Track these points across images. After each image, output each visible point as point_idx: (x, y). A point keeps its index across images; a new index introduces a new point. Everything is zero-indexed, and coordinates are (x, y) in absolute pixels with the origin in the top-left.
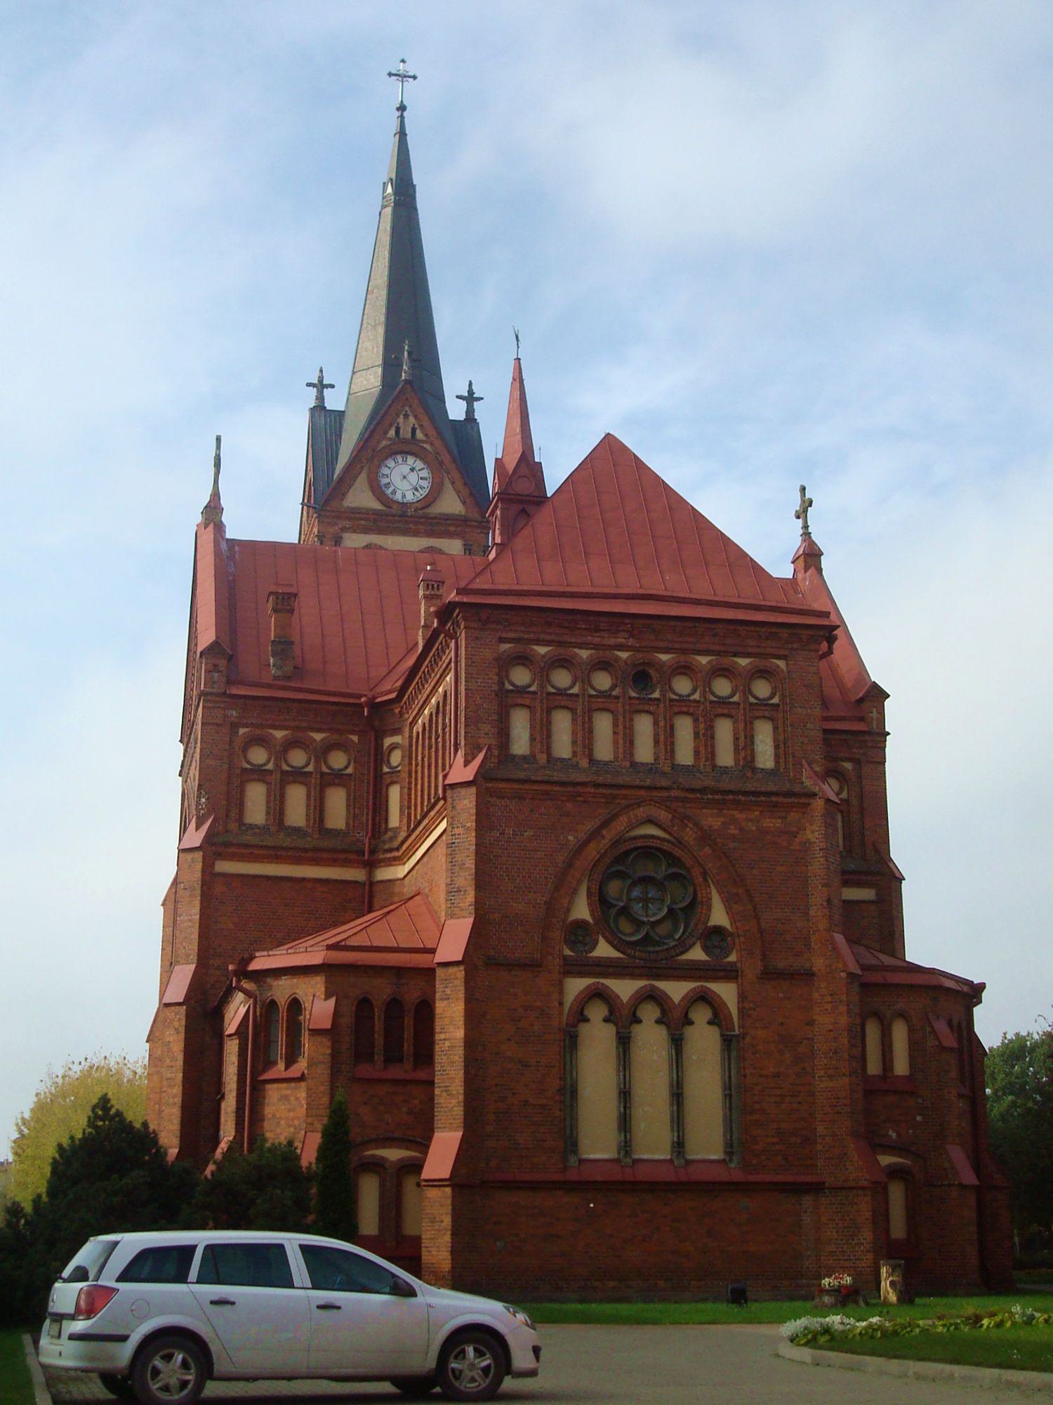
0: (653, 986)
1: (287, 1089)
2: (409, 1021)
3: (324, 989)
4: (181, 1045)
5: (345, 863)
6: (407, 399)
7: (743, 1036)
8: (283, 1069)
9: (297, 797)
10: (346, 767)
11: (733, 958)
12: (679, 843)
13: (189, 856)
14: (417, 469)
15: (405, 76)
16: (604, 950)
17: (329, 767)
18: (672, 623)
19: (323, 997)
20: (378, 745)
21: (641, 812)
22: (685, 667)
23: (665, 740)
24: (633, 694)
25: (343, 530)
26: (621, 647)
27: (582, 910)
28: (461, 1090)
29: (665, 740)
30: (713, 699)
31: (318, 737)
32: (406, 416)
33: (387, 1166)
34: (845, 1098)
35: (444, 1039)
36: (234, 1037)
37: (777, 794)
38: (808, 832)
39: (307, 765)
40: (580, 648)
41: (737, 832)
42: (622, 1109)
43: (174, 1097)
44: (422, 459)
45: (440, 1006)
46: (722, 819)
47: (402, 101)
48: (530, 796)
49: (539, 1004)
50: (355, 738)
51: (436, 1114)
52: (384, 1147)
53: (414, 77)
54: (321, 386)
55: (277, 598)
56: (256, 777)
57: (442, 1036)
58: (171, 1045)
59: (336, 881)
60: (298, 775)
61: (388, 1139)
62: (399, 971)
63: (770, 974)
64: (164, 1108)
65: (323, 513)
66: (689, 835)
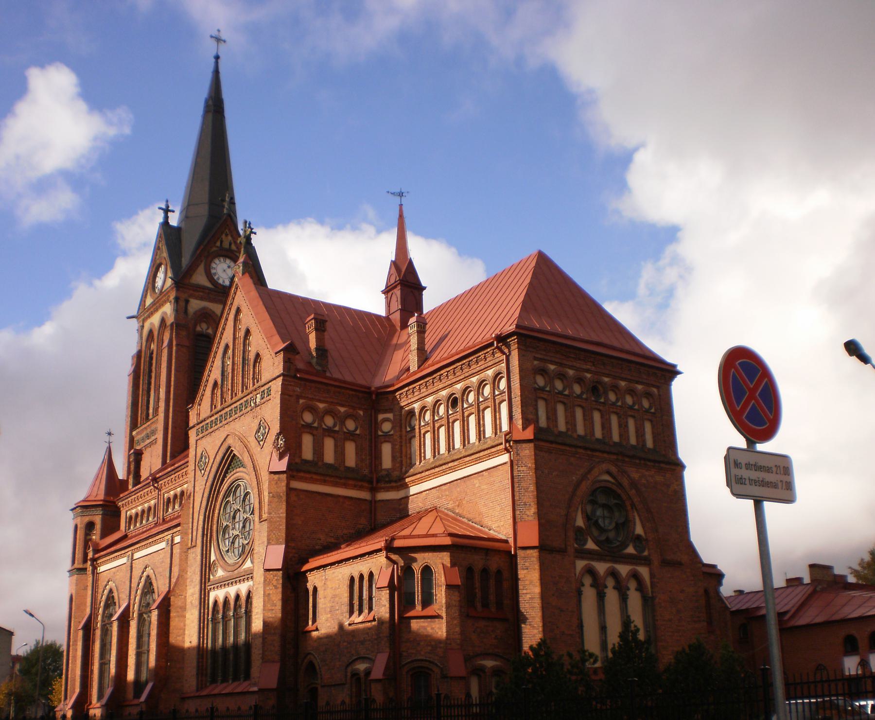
1: (424, 622)
2: (492, 582)
3: (449, 560)
4: (280, 596)
5: (360, 488)
6: (228, 225)
7: (653, 598)
8: (420, 610)
9: (329, 444)
10: (356, 430)
11: (646, 553)
12: (620, 485)
13: (276, 477)
16: (591, 545)
17: (347, 430)
20: (376, 418)
21: (604, 466)
24: (593, 399)
25: (192, 296)
26: (588, 371)
27: (580, 522)
28: (541, 624)
30: (303, 423)
31: (342, 409)
32: (227, 235)
33: (486, 671)
35: (526, 594)
36: (386, 589)
39: (335, 425)
40: (569, 368)
41: (645, 482)
42: (604, 638)
45: (521, 573)
47: (217, 53)
50: (361, 413)
51: (523, 638)
52: (484, 659)
56: (308, 430)
57: (525, 591)
58: (271, 596)
59: (359, 499)
60: (330, 432)
64: (266, 636)
66: (625, 482)
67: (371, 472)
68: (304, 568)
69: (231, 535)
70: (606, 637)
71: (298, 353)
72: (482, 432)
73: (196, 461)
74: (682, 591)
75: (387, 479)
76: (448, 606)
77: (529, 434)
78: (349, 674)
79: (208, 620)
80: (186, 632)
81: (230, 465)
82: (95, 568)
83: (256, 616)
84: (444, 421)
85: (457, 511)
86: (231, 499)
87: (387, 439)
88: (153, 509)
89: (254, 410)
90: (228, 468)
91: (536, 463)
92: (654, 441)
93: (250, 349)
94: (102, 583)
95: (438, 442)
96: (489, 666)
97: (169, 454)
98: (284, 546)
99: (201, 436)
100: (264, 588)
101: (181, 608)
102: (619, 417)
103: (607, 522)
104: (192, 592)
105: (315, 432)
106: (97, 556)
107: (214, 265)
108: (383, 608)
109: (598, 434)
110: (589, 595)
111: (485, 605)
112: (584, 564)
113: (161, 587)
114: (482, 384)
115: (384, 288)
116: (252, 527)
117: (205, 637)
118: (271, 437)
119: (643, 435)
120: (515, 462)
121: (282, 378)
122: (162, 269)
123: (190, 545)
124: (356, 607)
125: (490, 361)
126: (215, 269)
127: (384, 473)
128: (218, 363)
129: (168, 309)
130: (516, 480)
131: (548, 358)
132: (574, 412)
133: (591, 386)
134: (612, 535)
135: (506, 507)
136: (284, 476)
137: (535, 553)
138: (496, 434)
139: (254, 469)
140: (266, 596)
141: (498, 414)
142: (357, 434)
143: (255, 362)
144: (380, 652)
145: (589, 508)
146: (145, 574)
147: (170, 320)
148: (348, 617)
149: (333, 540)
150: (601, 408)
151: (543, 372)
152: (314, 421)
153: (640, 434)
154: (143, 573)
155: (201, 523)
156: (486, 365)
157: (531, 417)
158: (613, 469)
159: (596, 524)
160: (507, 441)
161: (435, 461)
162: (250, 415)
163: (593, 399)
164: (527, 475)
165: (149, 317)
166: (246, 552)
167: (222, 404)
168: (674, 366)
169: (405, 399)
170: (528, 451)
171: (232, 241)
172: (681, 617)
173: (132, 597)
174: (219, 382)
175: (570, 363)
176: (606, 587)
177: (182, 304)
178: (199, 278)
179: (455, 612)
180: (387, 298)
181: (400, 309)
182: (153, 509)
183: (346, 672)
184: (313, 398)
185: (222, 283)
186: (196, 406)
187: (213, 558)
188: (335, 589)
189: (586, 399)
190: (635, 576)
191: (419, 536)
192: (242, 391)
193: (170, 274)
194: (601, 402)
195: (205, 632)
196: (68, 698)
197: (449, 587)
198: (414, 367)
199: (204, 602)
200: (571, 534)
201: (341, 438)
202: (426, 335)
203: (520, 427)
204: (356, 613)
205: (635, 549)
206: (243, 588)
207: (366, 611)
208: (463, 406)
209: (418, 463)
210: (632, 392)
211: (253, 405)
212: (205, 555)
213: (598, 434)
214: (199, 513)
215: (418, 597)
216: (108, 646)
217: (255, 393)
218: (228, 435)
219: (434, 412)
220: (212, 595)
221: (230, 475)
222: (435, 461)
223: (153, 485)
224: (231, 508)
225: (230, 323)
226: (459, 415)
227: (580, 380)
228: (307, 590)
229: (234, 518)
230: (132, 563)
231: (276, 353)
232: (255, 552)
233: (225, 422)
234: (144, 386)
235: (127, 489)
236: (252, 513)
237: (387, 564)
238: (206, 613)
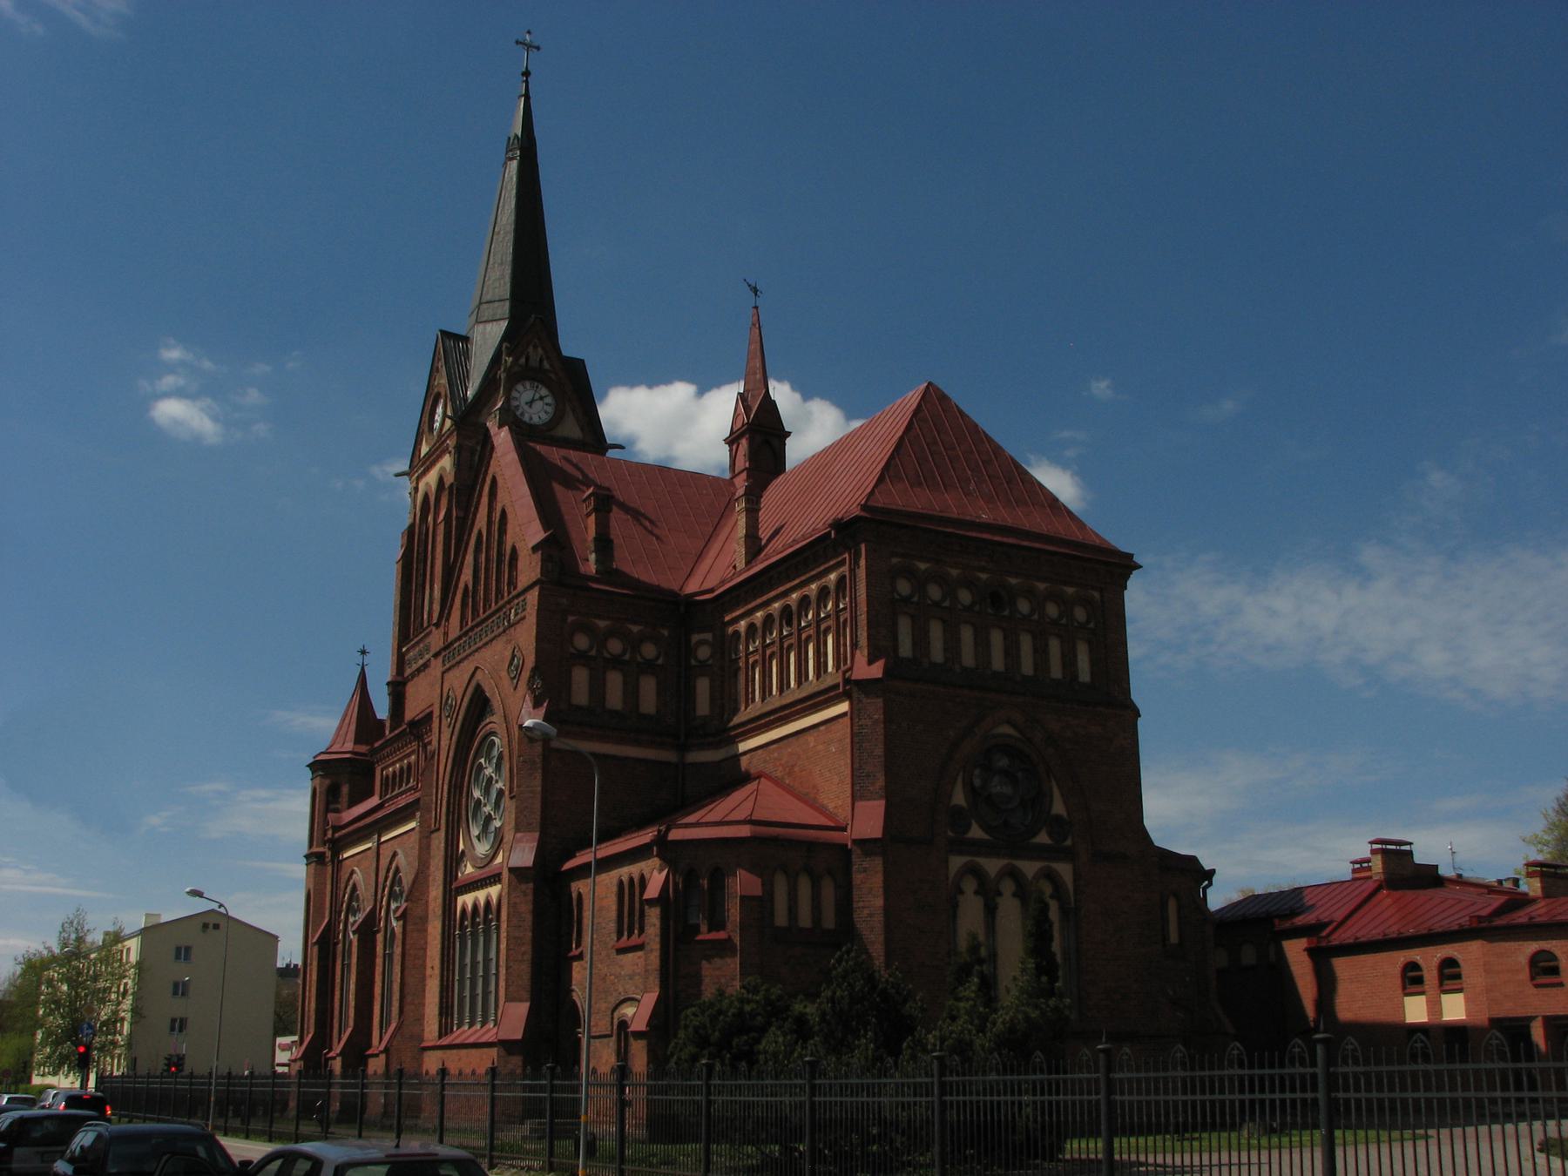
9: (615, 681)
10: (657, 658)
15: (530, 46)
16: (976, 832)
23: (1012, 652)
26: (983, 570)
27: (959, 798)
29: (1012, 652)
32: (535, 347)
35: (863, 907)
39: (624, 653)
43: (524, 954)
44: (548, 387)
50: (666, 633)
53: (538, 48)
57: (861, 904)
60: (616, 662)
64: (511, 964)
98: (537, 835)
99: (448, 666)
101: (421, 918)
115: (728, 435)
118: (526, 674)
126: (517, 399)
129: (446, 462)
139: (505, 719)
144: (647, 992)
147: (449, 480)
148: (616, 939)
153: (1069, 662)
168: (1130, 556)
171: (544, 356)
176: (1000, 894)
180: (731, 451)
181: (746, 469)
183: (612, 1018)
187: (461, 847)
198: (741, 565)
202: (760, 514)
209: (743, 708)
211: (506, 624)
212: (451, 842)
217: (508, 606)
225: (485, 500)
237: (660, 865)
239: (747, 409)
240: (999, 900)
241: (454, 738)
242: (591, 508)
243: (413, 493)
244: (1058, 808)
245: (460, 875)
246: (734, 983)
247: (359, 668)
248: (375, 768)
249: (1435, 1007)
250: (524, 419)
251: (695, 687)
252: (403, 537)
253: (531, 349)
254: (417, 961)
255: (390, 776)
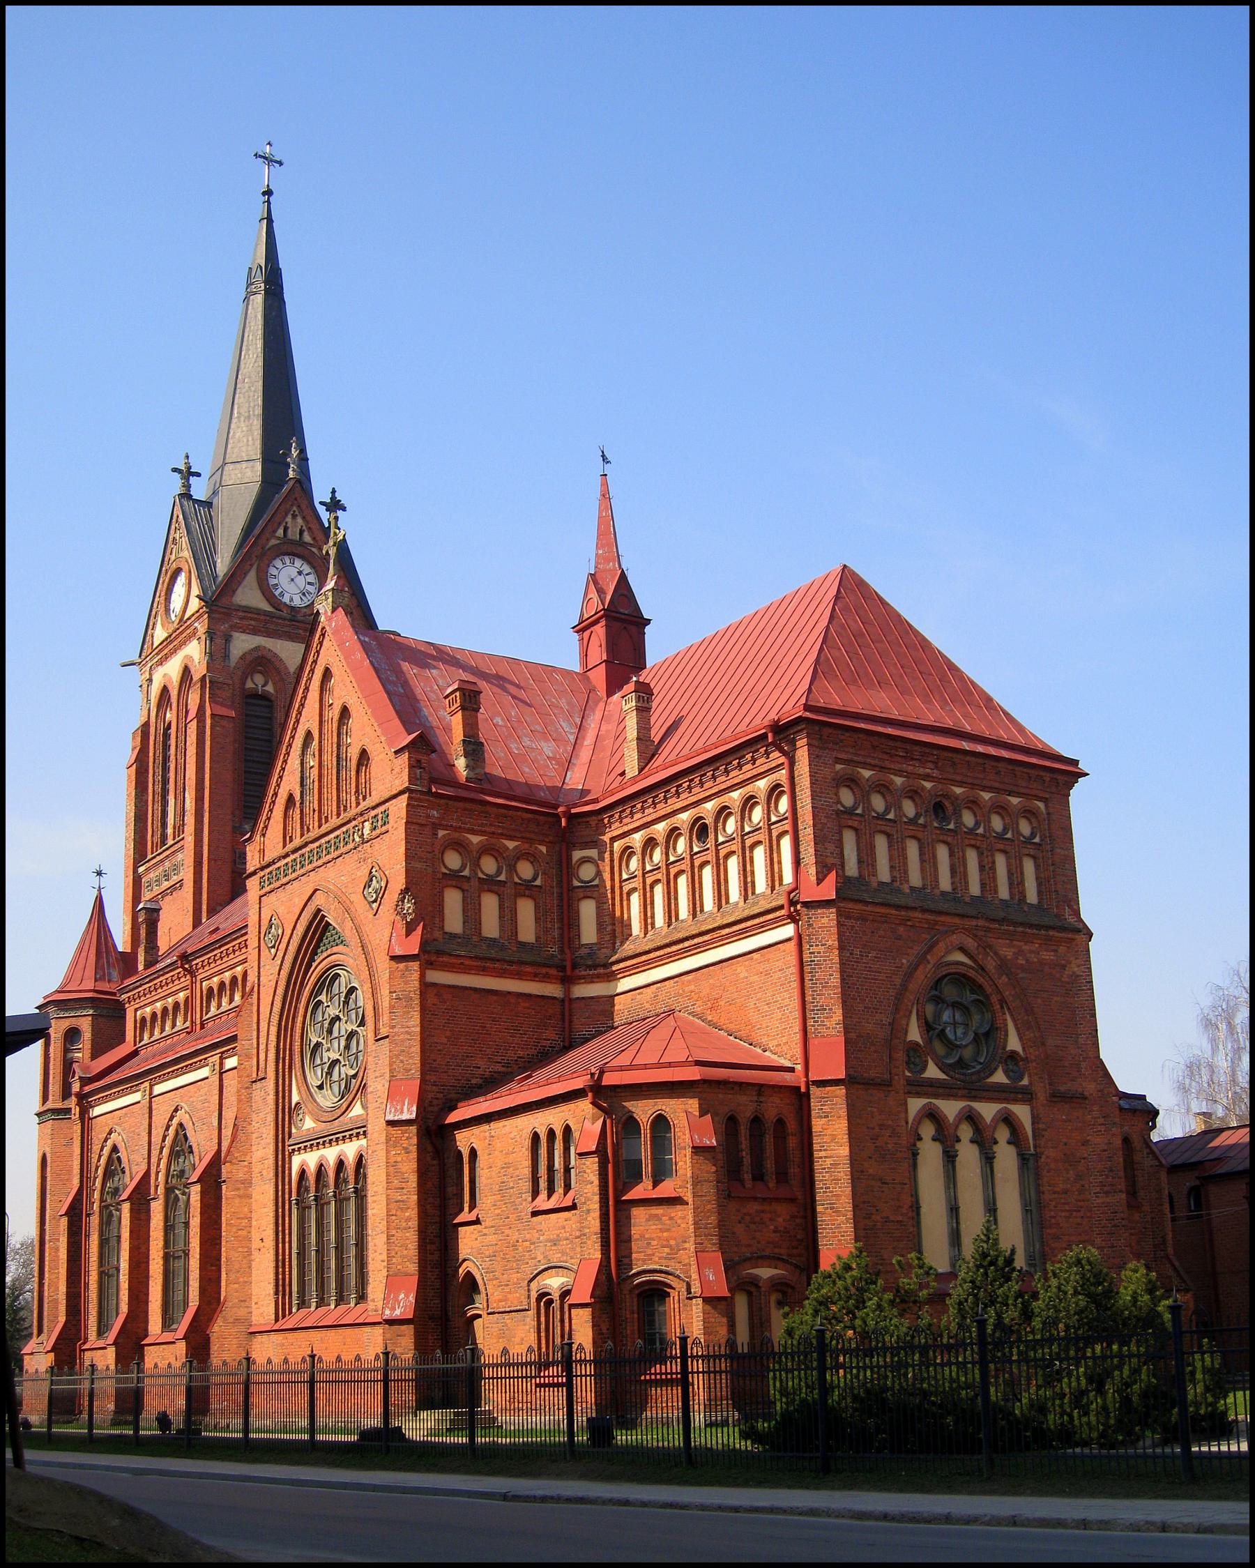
0: (971, 1108)
2: (769, 1140)
5: (545, 978)
6: (296, 499)
7: (1037, 1156)
9: (490, 904)
10: (535, 879)
11: (1025, 1082)
14: (305, 572)
16: (933, 1072)
17: (520, 878)
18: (968, 758)
19: (697, 1114)
20: (569, 858)
21: (955, 939)
22: (974, 802)
23: (958, 870)
24: (936, 825)
25: (235, 628)
26: (927, 777)
27: (914, 1034)
29: (958, 870)
31: (511, 845)
32: (294, 516)
34: (1122, 1212)
37: (1053, 928)
38: (1073, 966)
39: (499, 872)
42: (955, 1225)
43: (408, 1219)
44: (309, 563)
45: (817, 1124)
46: (1013, 950)
48: (871, 918)
49: (890, 1122)
50: (543, 849)
53: (280, 163)
54: (188, 474)
55: (464, 695)
56: (454, 883)
57: (822, 1154)
60: (490, 884)
61: (762, 1257)
62: (760, 1088)
63: (1058, 1097)
65: (214, 608)
66: (991, 964)
67: (562, 951)
68: (453, 1117)
69: (325, 1060)
70: (958, 1223)
71: (434, 751)
72: (749, 885)
73: (260, 932)
74: (1085, 1143)
75: (590, 963)
76: (696, 1181)
77: (828, 890)
78: (534, 1295)
79: (290, 1202)
80: (254, 1223)
81: (320, 940)
82: (84, 1112)
83: (375, 1198)
84: (685, 865)
85: (710, 1018)
86: (323, 997)
87: (589, 894)
88: (182, 1006)
89: (360, 849)
90: (317, 946)
91: (840, 940)
92: (1039, 893)
93: (349, 741)
94: (98, 1135)
95: (676, 899)
96: (765, 1277)
97: (204, 907)
99: (267, 889)
100: (388, 1152)
102: (980, 854)
103: (960, 1031)
104: (262, 1151)
105: (466, 886)
106: (87, 1089)
107: (272, 571)
108: (589, 1186)
109: (945, 883)
110: (930, 1153)
111: (759, 1177)
112: (921, 1105)
113: (203, 1143)
114: (749, 803)
116: (361, 1047)
117: (287, 1232)
119: (1022, 883)
120: (805, 939)
121: (407, 795)
122: (182, 579)
123: (254, 1075)
124: (543, 1184)
125: (762, 764)
127: (584, 951)
128: (294, 762)
129: (194, 651)
130: (807, 969)
131: (860, 759)
132: (904, 849)
133: (933, 803)
134: (968, 1053)
135: (791, 1012)
136: (415, 965)
137: (841, 1091)
138: (773, 889)
140: (391, 1165)
141: (775, 855)
142: (536, 886)
143: (359, 765)
145: (930, 1009)
146: (175, 1121)
147: (199, 670)
149: (499, 1068)
150: (949, 839)
151: (851, 782)
152: (463, 867)
153: (1016, 881)
154: (171, 1118)
155: (273, 1038)
156: (755, 772)
157: (830, 860)
158: (970, 943)
159: (942, 1035)
160: (792, 903)
161: (671, 933)
162: (354, 856)
163: (936, 825)
164: (825, 961)
165: (161, 663)
166: (354, 1089)
167: (302, 835)
168: (1075, 763)
169: (617, 824)
170: (827, 920)
172: (1083, 1186)
173: (154, 1160)
174: (297, 797)
175: (897, 767)
177: (219, 641)
178: (248, 596)
179: (709, 1190)
180: (581, 640)
182: (182, 1006)
184: (460, 827)
185: (288, 602)
186: (258, 838)
188: (507, 1154)
189: (924, 826)
190: (1008, 1120)
191: (645, 1067)
192: (338, 815)
193: (196, 590)
194: (949, 830)
195: (287, 1221)
196: (45, 1329)
197: (697, 1150)
198: (632, 768)
199: (283, 1172)
200: (900, 1056)
201: (510, 892)
203: (813, 878)
204: (543, 1195)
205: (1008, 1077)
206: (350, 1150)
207: (560, 1190)
208: (716, 840)
210: (1001, 809)
211: (357, 839)
212: (282, 1093)
213: (945, 883)
214: (269, 1021)
215: (647, 1168)
216: (113, 1242)
217: (360, 819)
218: (316, 890)
219: (667, 848)
220: (296, 1161)
221: (321, 958)
222: (671, 933)
223: (182, 967)
224: (323, 1013)
226: (710, 856)
227: (913, 794)
228: (460, 1154)
229: (330, 1032)
230: (150, 1102)
231: (396, 752)
232: (369, 1090)
233: (311, 867)
234: (156, 787)
235: (135, 971)
236: (362, 1024)
238: (287, 1191)
239: (601, 592)
240: (958, 1146)
241: (284, 973)
242: (456, 706)
243: (145, 686)
244: (1014, 1043)
245: (294, 1130)
246: (687, 1245)
247: (95, 893)
248: (125, 1010)
249: (695, 1280)
250: (284, 600)
251: (578, 912)
252: (134, 738)
253: (289, 519)
254: (240, 1232)
255: (148, 1019)
